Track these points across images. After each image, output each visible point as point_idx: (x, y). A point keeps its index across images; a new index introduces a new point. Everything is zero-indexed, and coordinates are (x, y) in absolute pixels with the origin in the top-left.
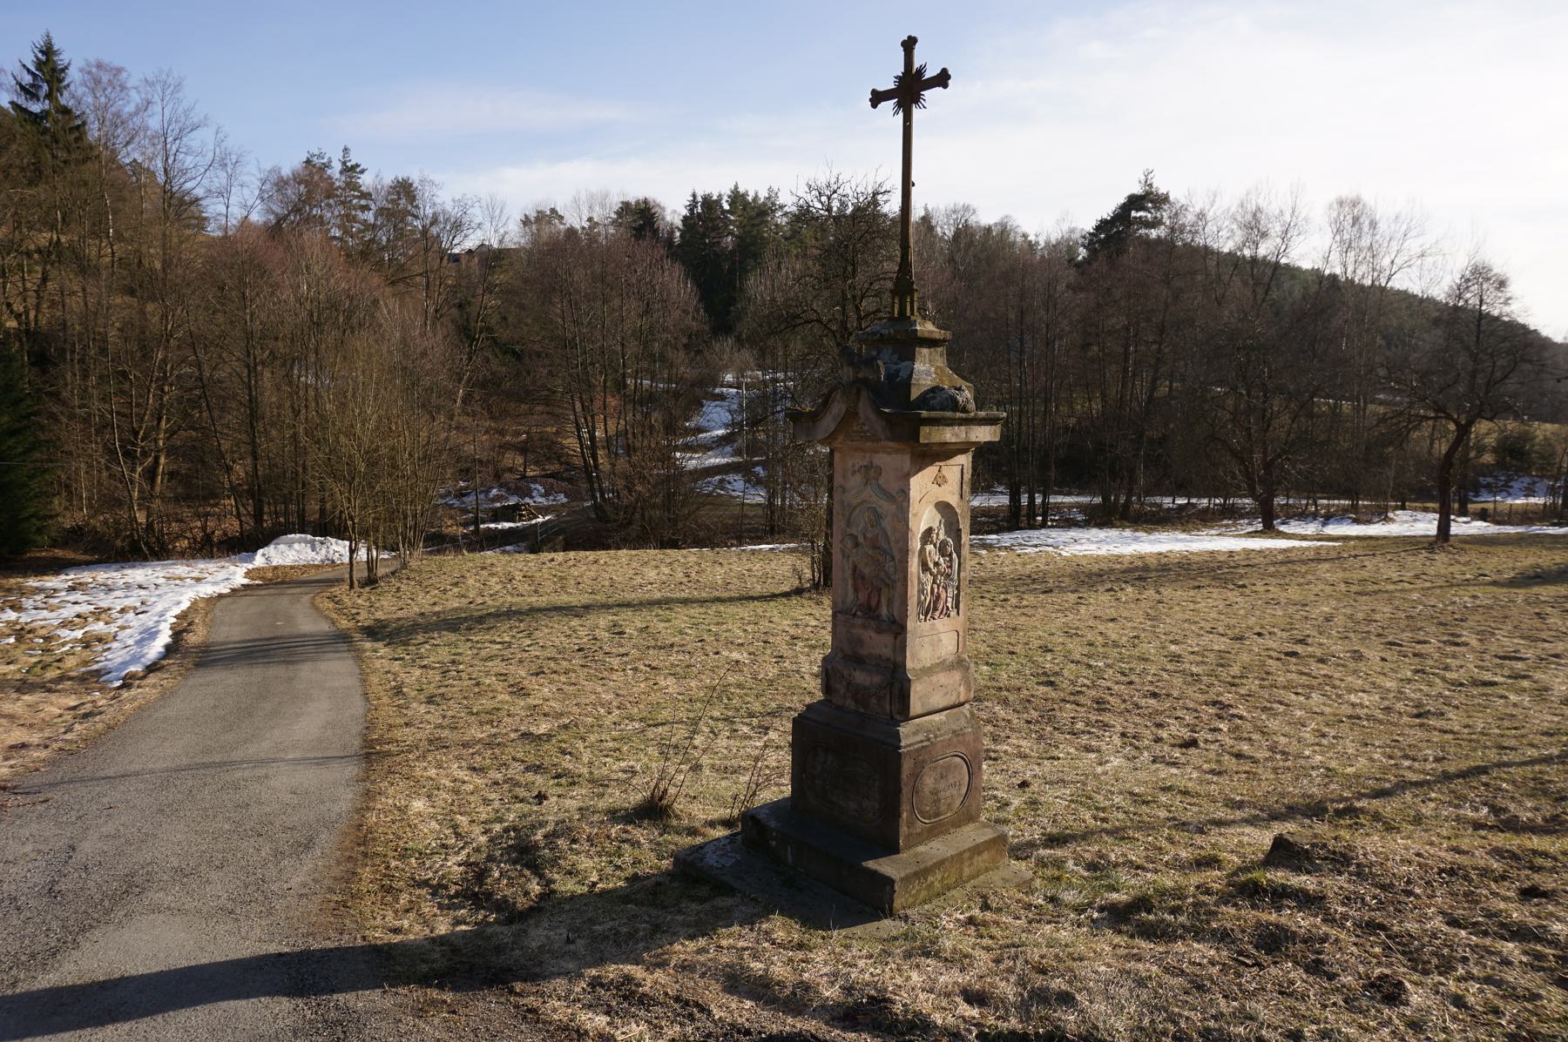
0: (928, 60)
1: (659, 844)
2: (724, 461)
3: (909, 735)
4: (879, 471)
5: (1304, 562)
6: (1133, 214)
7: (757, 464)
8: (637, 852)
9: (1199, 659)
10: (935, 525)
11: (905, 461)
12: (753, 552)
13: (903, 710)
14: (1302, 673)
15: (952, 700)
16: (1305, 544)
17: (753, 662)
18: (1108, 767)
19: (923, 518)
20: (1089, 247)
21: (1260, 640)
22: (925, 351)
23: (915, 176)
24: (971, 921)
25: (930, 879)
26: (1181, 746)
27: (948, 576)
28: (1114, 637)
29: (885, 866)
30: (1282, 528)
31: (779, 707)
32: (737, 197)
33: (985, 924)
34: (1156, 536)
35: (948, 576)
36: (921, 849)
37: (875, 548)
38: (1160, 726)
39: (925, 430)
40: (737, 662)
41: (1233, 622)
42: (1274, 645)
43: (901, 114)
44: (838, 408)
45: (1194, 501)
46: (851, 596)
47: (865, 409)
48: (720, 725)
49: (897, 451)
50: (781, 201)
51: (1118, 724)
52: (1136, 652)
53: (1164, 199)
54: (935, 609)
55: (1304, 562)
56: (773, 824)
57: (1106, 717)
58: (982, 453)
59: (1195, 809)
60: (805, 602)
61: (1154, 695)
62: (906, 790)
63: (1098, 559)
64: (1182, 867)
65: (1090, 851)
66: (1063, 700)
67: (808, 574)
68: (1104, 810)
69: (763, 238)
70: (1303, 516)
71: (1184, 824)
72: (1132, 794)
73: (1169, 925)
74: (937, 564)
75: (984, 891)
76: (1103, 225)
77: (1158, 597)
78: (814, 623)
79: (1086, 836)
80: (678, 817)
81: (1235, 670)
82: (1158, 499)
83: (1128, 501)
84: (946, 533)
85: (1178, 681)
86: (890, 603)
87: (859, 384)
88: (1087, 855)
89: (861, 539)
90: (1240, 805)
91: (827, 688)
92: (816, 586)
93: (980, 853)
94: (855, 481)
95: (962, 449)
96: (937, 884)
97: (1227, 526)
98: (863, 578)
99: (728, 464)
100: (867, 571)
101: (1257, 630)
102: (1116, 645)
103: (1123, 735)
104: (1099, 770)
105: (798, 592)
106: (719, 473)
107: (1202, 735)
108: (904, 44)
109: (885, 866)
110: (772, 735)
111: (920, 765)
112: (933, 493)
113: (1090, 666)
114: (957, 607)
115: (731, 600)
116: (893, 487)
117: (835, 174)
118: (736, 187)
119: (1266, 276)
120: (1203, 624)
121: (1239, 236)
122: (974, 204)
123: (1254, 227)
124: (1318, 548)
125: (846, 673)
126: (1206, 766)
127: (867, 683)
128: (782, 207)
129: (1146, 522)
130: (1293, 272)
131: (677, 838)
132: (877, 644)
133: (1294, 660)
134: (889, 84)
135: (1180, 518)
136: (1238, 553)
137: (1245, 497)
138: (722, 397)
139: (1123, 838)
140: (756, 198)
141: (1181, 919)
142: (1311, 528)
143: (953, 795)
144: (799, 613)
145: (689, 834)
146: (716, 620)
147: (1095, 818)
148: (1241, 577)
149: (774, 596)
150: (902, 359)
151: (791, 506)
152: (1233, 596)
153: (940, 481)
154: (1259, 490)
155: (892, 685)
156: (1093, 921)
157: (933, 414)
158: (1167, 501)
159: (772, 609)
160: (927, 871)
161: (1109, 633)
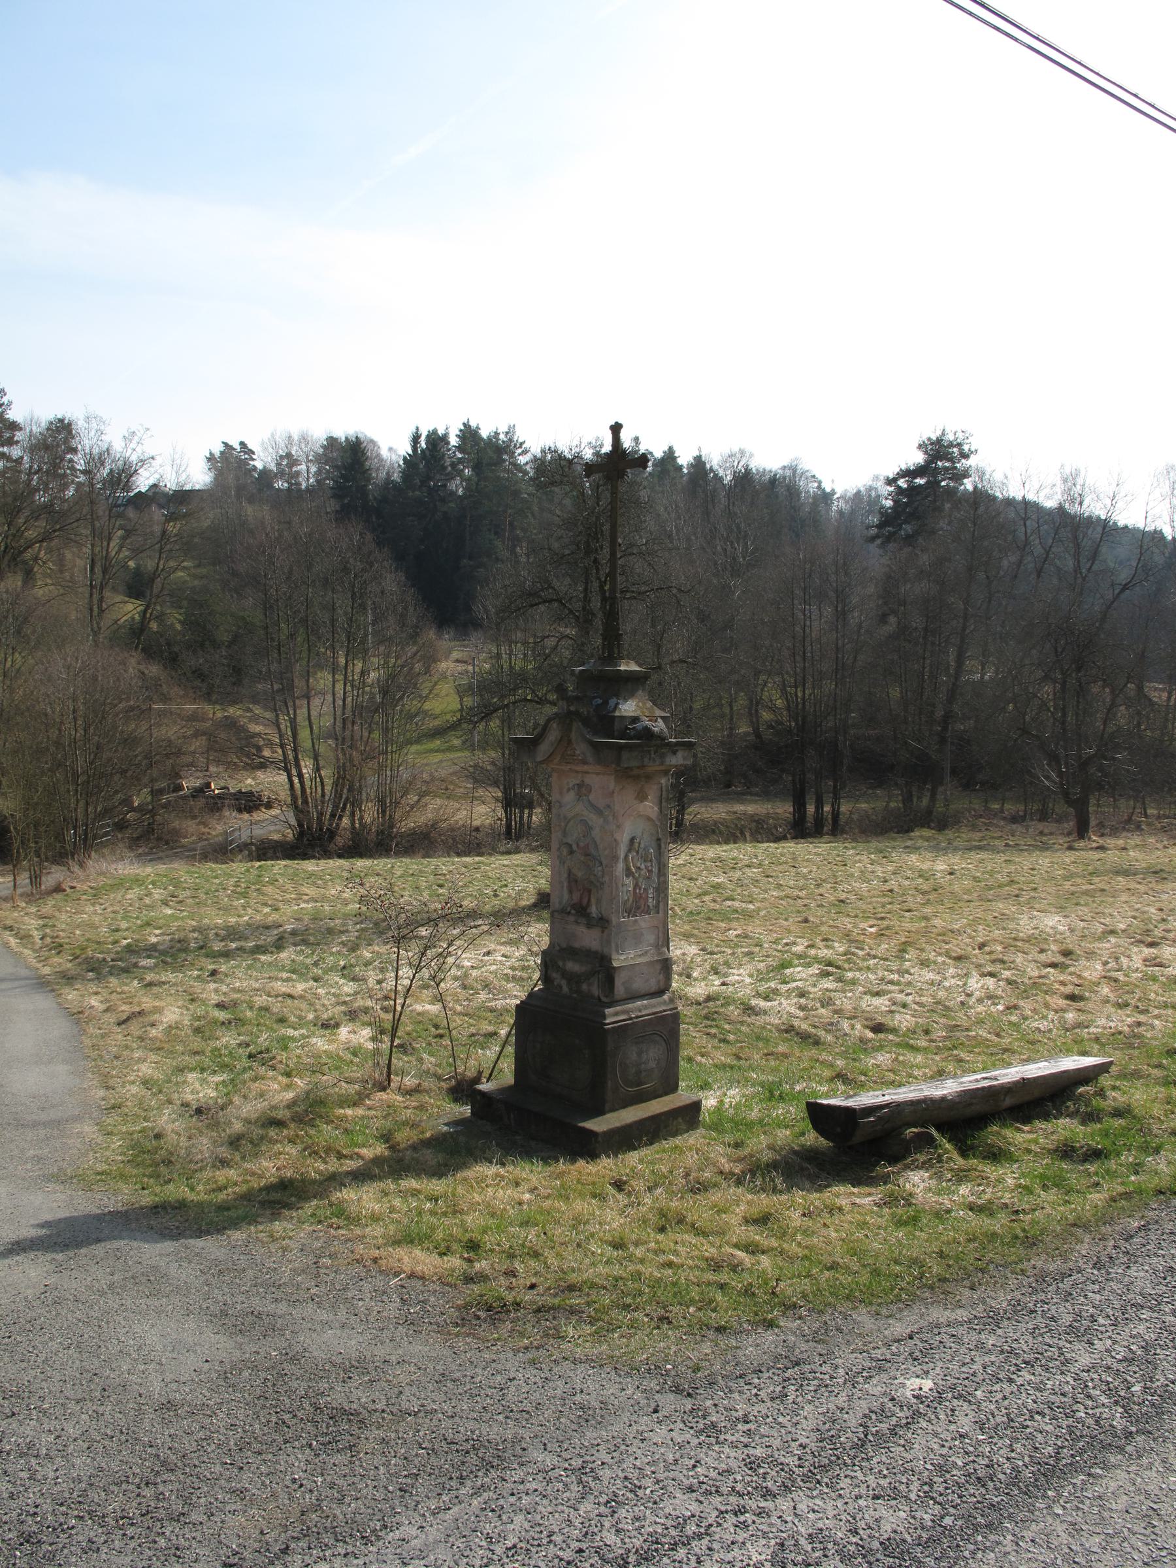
32: (469, 434)
37: (587, 855)
44: (553, 735)
46: (566, 896)
86: (599, 901)
89: (575, 847)
94: (570, 797)
100: (579, 874)
122: (748, 448)
132: (588, 938)
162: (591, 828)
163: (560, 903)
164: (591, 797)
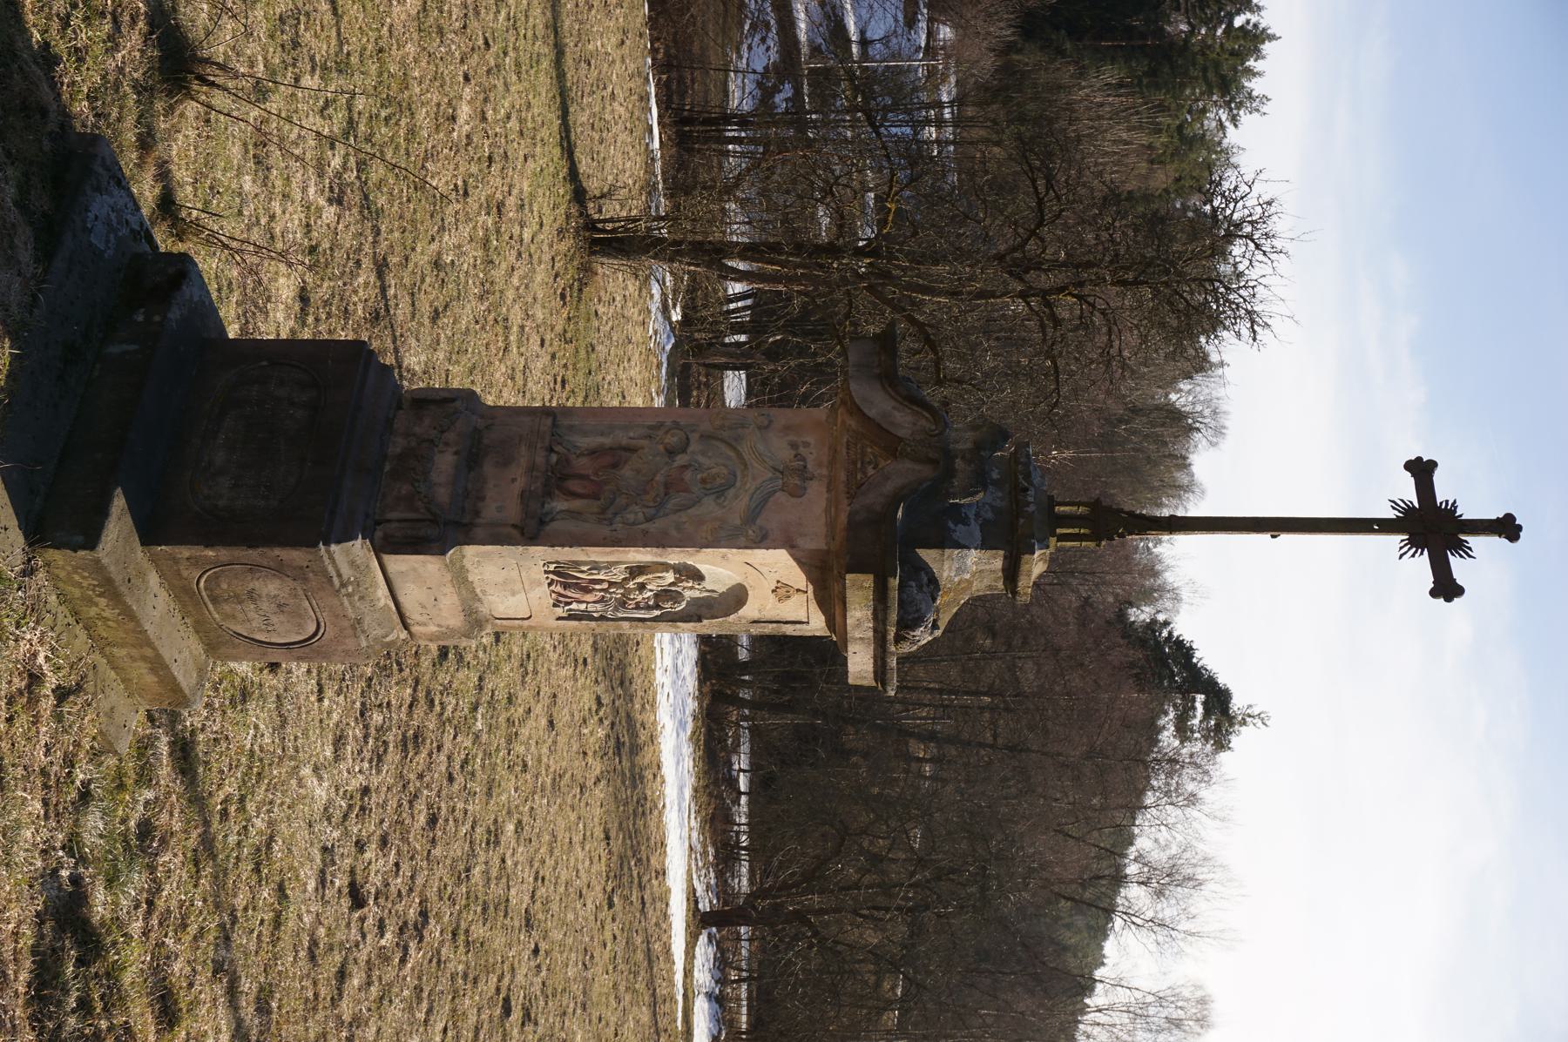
0: (1481, 562)
1: (117, 86)
2: (803, 37)
3: (351, 556)
4: (798, 492)
5: (651, 984)
6: (1200, 698)
7: (798, 92)
8: (98, 49)
9: (494, 873)
10: (707, 584)
11: (815, 541)
12: (644, 98)
13: (386, 546)
14: (477, 1030)
15: (413, 614)
16: (679, 978)
17: (455, 148)
18: (312, 782)
19: (720, 568)
20: (1153, 626)
21: (527, 954)
22: (998, 564)
23: (1286, 539)
24: (35, 678)
25: (103, 602)
26: (352, 885)
27: (622, 604)
28: (524, 732)
29: (118, 527)
30: (703, 939)
31: (380, 212)
32: (1254, 39)
33: (33, 701)
34: (687, 750)
35: (622, 604)
36: (154, 579)
37: (667, 486)
38: (384, 842)
39: (868, 581)
40: (453, 118)
41: (555, 907)
42: (520, 978)
43: (1391, 514)
44: (904, 422)
45: (744, 799)
46: (585, 442)
47: (902, 473)
48: (340, 116)
49: (831, 525)
50: (1245, 117)
51: (384, 778)
52: (502, 771)
53: (1221, 745)
54: (566, 586)
55: (651, 984)
56: (175, 314)
57: (393, 756)
58: (825, 654)
59: (252, 947)
60: (562, 210)
61: (433, 820)
62: (253, 554)
63: (648, 671)
64: (156, 970)
65: (172, 820)
66: (417, 681)
67: (611, 209)
68: (242, 809)
69: (1183, 86)
70: (722, 963)
71: (227, 938)
72: (271, 839)
73: (59, 1004)
74: (642, 587)
75: (89, 687)
76: (1183, 651)
77: (590, 783)
78: (527, 236)
79: (197, 801)
80: (170, 110)
81: (478, 931)
82: (745, 748)
83: (742, 703)
84: (694, 601)
85: (458, 849)
86: (574, 515)
87: (943, 460)
88: (164, 817)
89: (681, 460)
90: (263, 1008)
91: (428, 402)
92: (591, 225)
93: (153, 670)
94: (780, 449)
96: (93, 611)
97: (705, 853)
98: (615, 466)
99: (796, 42)
100: (627, 472)
101: (543, 946)
102: (511, 739)
103: (366, 791)
104: (306, 771)
105: (579, 195)
106: (780, 22)
107: (372, 911)
108: (1509, 518)
109: (118, 527)
110: (330, 213)
111: (300, 574)
112: (767, 586)
113: (475, 708)
114: (570, 617)
115: (561, 76)
116: (771, 520)
117: (1289, 246)
118: (1272, 38)
119: (1095, 901)
120: (550, 862)
121: (1157, 857)
122: (1227, 444)
123: (1170, 878)
124: (673, 999)
125: (450, 436)
126: (322, 931)
127: (434, 476)
128: (1234, 120)
129: (709, 732)
130: (1101, 933)
131: (130, 120)
132: (504, 493)
133: (498, 1011)
134: (1444, 491)
135: (716, 783)
136: (662, 883)
137: (751, 881)
138: (911, 22)
139: (196, 863)
140: (1251, 73)
141: (72, 1021)
142: (703, 977)
143: (251, 621)
144: (542, 204)
145: (140, 137)
146: (524, 58)
147: (225, 801)
148: (626, 898)
149: (568, 150)
150: (985, 526)
151: (727, 153)
152: (596, 896)
153: (782, 591)
154: (762, 904)
155: (434, 521)
156: (55, 871)
157: (894, 595)
158: (742, 761)
159: (548, 156)
160: (115, 597)
161: (531, 723)
162: (720, 493)
163: (571, 428)
164: (781, 497)
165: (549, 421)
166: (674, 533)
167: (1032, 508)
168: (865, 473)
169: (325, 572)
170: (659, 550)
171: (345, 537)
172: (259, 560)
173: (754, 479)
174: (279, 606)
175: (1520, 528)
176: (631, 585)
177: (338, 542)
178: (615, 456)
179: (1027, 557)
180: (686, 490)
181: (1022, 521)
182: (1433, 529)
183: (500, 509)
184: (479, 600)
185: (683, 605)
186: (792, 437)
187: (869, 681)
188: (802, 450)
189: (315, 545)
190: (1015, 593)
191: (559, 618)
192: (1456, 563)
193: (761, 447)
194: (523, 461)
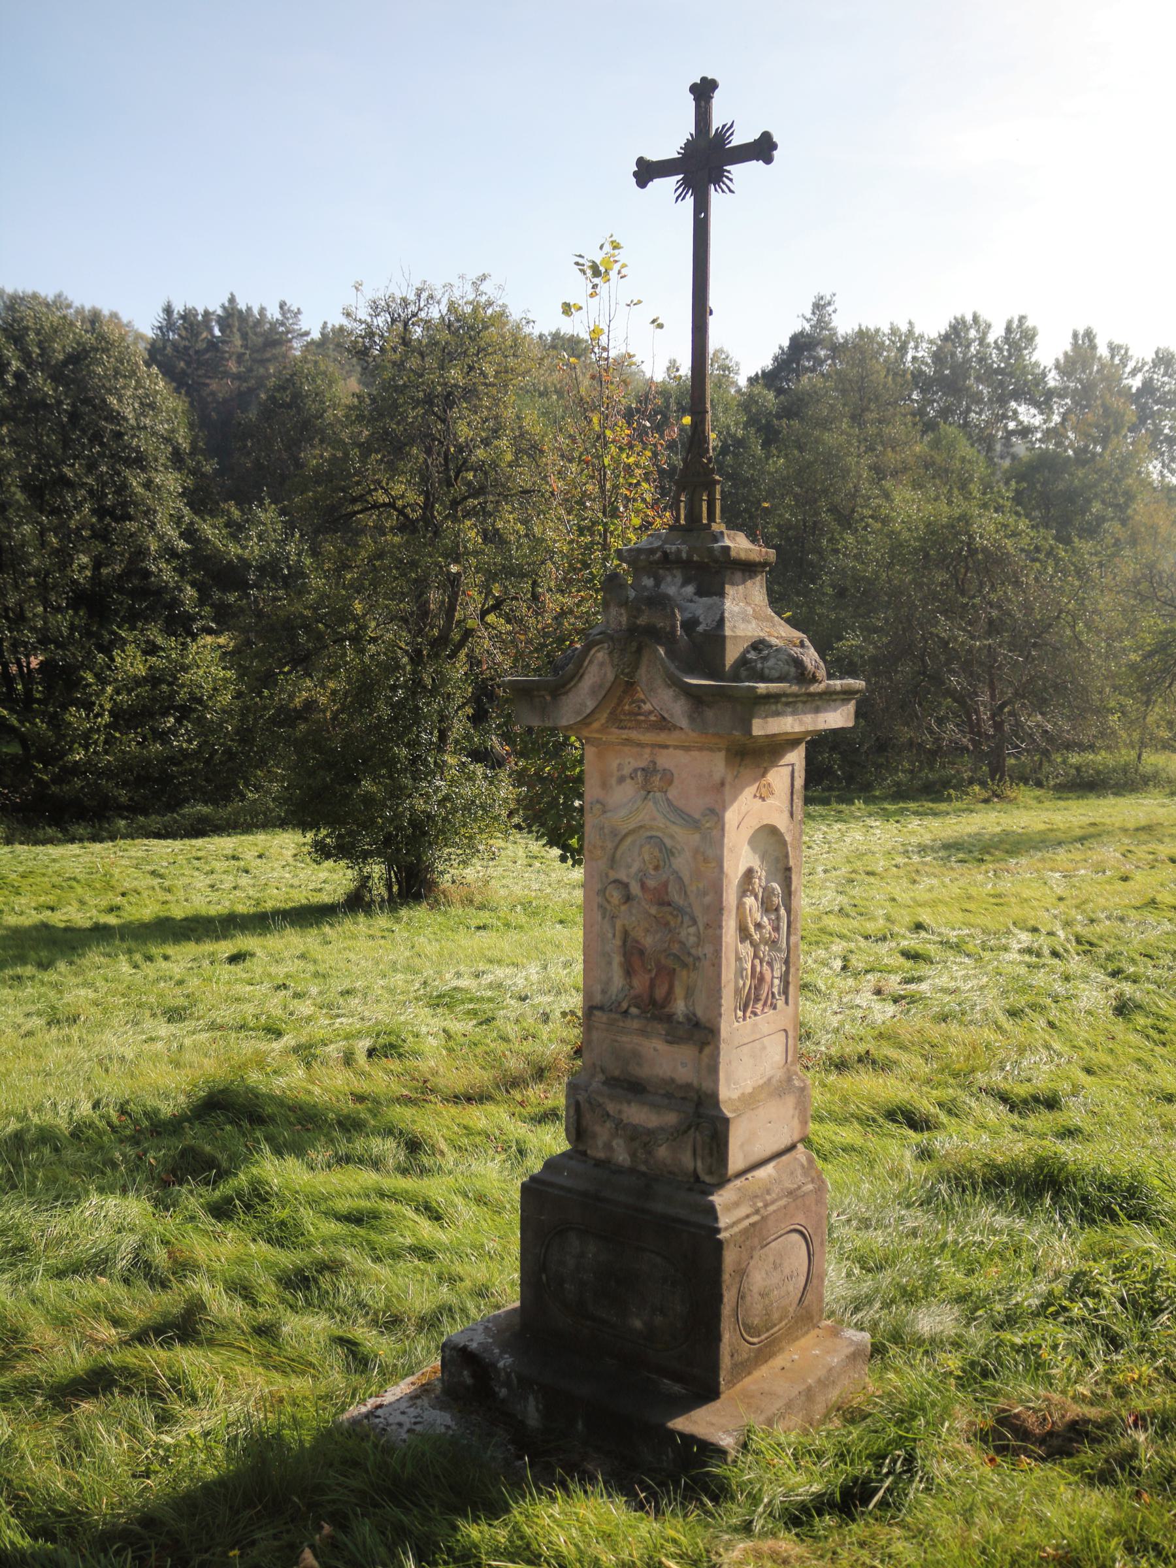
0: (737, 117)
3: (730, 1208)
4: (668, 778)
11: (717, 765)
23: (713, 302)
27: (773, 944)
29: (700, 1422)
35: (773, 944)
43: (690, 201)
46: (618, 980)
56: (505, 1362)
86: (689, 993)
89: (635, 889)
94: (623, 794)
95: (792, 742)
98: (642, 953)
100: (648, 941)
108: (694, 89)
109: (700, 1422)
114: (785, 992)
118: (232, 300)
125: (611, 1107)
132: (666, 1061)
162: (670, 853)
163: (604, 992)
164: (672, 793)
165: (597, 1013)
166: (708, 899)
167: (684, 548)
168: (650, 712)
169: (745, 1231)
170: (725, 913)
171: (711, 1211)
172: (734, 1291)
173: (654, 819)
174: (775, 1268)
175: (704, 79)
176: (756, 937)
177: (716, 1219)
178: (633, 955)
179: (733, 554)
180: (665, 885)
181: (695, 558)
182: (704, 163)
183: (684, 1065)
184: (770, 1080)
185: (775, 885)
186: (613, 781)
187: (851, 707)
188: (626, 771)
189: (720, 1243)
190: (765, 564)
191: (787, 1003)
192: (738, 139)
193: (623, 813)
194: (637, 1040)
